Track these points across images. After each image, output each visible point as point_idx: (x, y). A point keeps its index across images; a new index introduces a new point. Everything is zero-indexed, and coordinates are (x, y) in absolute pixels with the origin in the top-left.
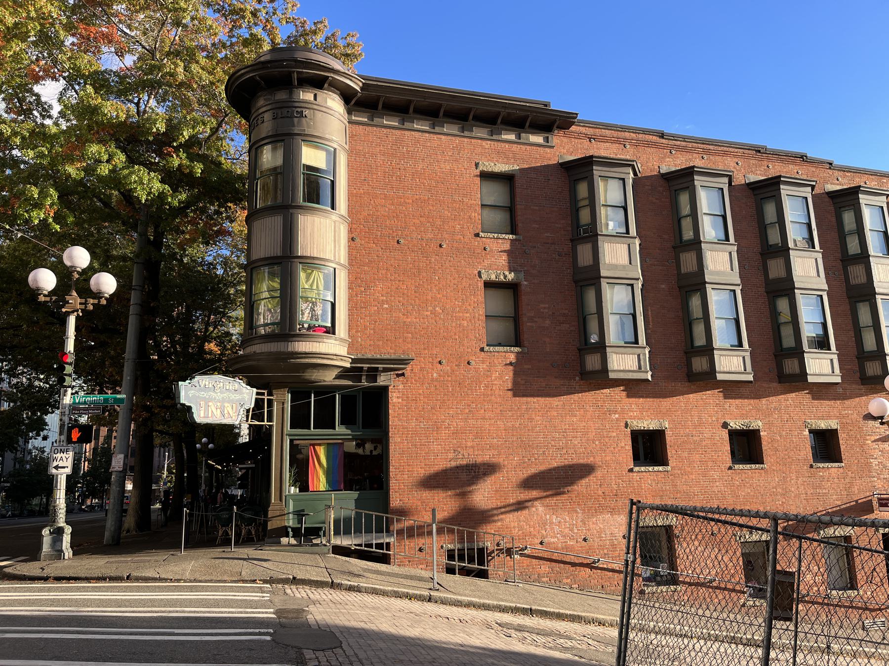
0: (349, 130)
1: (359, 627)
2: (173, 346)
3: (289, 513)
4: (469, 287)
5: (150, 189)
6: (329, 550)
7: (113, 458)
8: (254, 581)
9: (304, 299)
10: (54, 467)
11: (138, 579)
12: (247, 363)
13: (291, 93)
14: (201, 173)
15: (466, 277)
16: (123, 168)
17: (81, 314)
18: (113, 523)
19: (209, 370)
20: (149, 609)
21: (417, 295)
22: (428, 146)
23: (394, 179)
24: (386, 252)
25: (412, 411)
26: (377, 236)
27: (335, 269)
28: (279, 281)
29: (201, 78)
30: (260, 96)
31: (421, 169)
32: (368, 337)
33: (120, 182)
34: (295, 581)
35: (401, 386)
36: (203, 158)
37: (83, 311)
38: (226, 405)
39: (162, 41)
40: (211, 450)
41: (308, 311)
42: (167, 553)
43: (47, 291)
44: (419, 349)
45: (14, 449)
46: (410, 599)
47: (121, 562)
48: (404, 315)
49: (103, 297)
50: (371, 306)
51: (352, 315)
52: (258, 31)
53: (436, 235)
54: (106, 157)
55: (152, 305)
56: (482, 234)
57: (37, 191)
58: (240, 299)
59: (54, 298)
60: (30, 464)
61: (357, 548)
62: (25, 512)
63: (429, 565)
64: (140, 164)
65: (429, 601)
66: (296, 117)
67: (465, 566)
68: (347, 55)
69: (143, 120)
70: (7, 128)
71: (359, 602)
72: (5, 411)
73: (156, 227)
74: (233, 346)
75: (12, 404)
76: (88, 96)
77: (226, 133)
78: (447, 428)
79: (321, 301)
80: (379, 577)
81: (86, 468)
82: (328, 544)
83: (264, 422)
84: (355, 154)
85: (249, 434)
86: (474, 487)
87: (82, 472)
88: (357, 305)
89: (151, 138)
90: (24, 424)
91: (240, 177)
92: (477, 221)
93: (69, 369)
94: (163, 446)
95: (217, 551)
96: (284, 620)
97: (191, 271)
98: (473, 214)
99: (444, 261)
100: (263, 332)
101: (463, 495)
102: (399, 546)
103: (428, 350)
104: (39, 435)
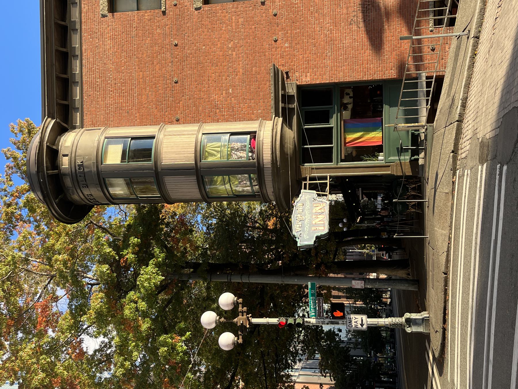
0: (88, 127)
1: (500, 94)
2: (272, 250)
3: (400, 160)
4: (210, 18)
5: (154, 273)
6: (430, 126)
7: (355, 287)
8: (454, 183)
9: (229, 157)
10: (362, 327)
11: (447, 267)
12: (282, 197)
13: (65, 175)
14: (138, 238)
15: (201, 21)
16: (140, 292)
17: (250, 315)
18: (403, 285)
19: (288, 225)
20: (473, 258)
21: (219, 64)
22: (93, 60)
23: (124, 88)
24: (185, 92)
25: (318, 64)
26: (173, 100)
27: (203, 134)
28: (216, 177)
29: (64, 242)
30: (71, 198)
31: (113, 65)
32: (257, 104)
33: (151, 294)
34: (455, 151)
35: (297, 74)
36: (126, 238)
37: (248, 314)
38: (314, 211)
39: (42, 270)
40: (348, 220)
41: (238, 153)
42: (427, 248)
43: (234, 338)
44: (265, 60)
45: (348, 350)
46: (476, 55)
47: (433, 278)
48: (237, 75)
49: (237, 301)
50: (231, 103)
51: (240, 118)
52: (21, 202)
53: (168, 50)
54: (133, 305)
55: (241, 267)
56: (163, 9)
57: (162, 348)
58: (234, 206)
59: (240, 333)
60: (358, 339)
61: (429, 103)
62: (391, 340)
63: (446, 41)
64: (135, 281)
65: (478, 38)
66: (84, 169)
67: (449, 11)
68: (29, 132)
69: (101, 281)
70: (119, 371)
71: (476, 97)
72: (321, 357)
73: (183, 268)
74: (270, 209)
75: (317, 352)
76: (89, 319)
77: (105, 222)
78: (331, 32)
79: (229, 144)
80: (455, 83)
81: (361, 303)
82: (426, 127)
83: (327, 182)
84: (108, 121)
85: (336, 194)
86: (381, 5)
87: (364, 305)
88: (231, 115)
89: (115, 275)
90: (330, 344)
91: (138, 210)
92: (152, 13)
93: (291, 321)
94: (345, 253)
95: (428, 212)
96: (489, 157)
97: (215, 241)
98: (146, 17)
99: (189, 41)
100: (257, 187)
101: (388, 14)
102: (429, 69)
103: (265, 52)
104: (338, 334)
